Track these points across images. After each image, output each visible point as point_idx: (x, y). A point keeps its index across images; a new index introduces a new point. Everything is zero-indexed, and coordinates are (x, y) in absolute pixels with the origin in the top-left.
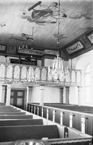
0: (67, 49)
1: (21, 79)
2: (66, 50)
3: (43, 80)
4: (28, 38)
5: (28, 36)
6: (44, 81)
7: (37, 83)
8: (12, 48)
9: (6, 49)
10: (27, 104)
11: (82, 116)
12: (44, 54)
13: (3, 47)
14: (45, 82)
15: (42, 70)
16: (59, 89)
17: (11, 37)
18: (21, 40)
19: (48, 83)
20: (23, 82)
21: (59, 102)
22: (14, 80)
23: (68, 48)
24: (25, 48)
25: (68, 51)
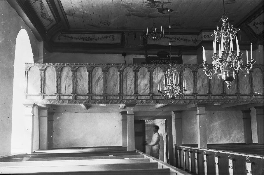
0: (251, 25)
1: (153, 93)
2: (249, 27)
3: (201, 93)
4: (161, 10)
5: (161, 5)
6: (203, 95)
7: (188, 101)
8: (135, 36)
9: (123, 40)
10: (174, 147)
11: (215, 154)
12: (200, 41)
13: (116, 36)
14: (207, 97)
15: (197, 72)
16: (241, 112)
17: (128, 12)
18: (150, 17)
19: (213, 100)
20: (159, 100)
21: (242, 141)
22: (139, 98)
23: (253, 22)
24: (158, 32)
25: (253, 28)
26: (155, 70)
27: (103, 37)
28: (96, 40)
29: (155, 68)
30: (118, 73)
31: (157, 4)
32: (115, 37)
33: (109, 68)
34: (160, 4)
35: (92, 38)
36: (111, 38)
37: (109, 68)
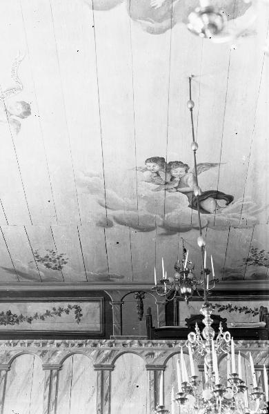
13: (86, 306)
26: (169, 363)
27: (48, 313)
28: (30, 320)
29: (171, 356)
30: (45, 374)
31: (177, 172)
32: (84, 312)
33: (15, 358)
34: (186, 171)
35: (19, 315)
36: (72, 312)
37: (15, 358)
